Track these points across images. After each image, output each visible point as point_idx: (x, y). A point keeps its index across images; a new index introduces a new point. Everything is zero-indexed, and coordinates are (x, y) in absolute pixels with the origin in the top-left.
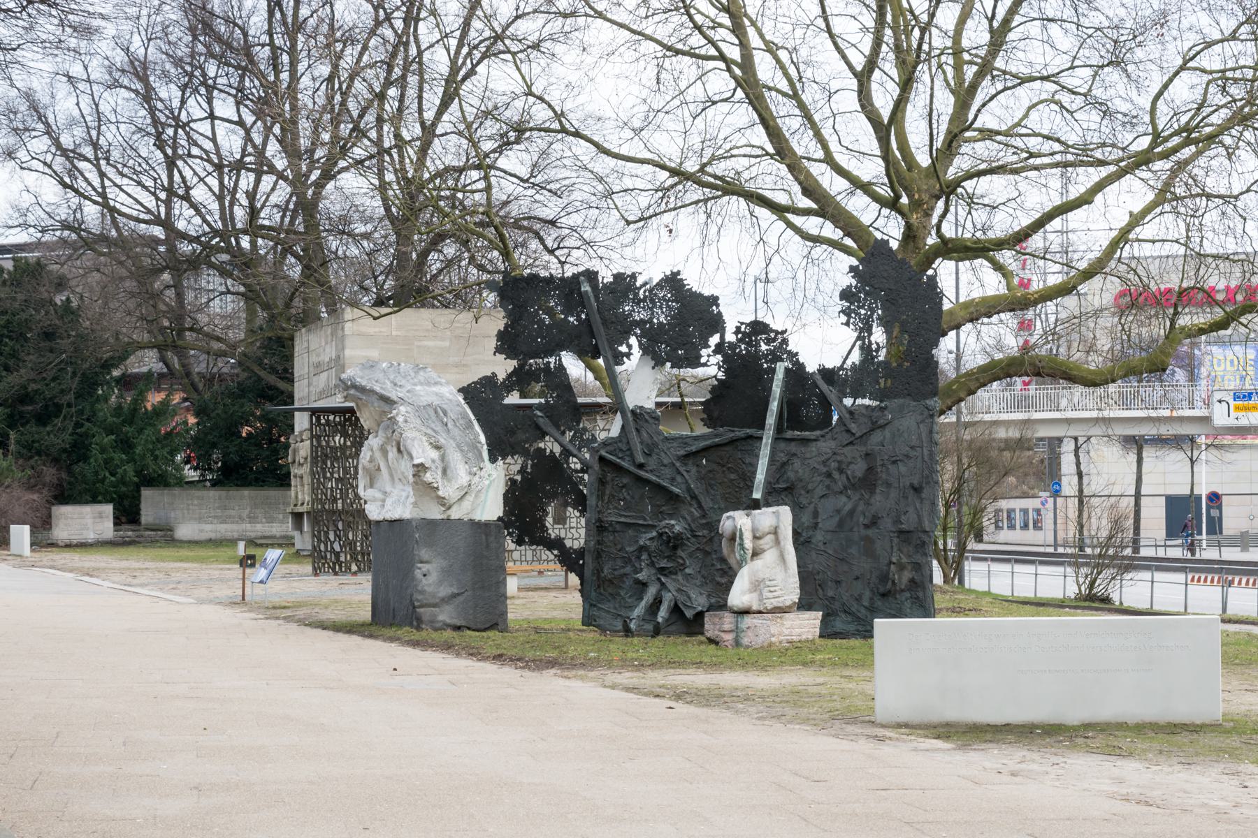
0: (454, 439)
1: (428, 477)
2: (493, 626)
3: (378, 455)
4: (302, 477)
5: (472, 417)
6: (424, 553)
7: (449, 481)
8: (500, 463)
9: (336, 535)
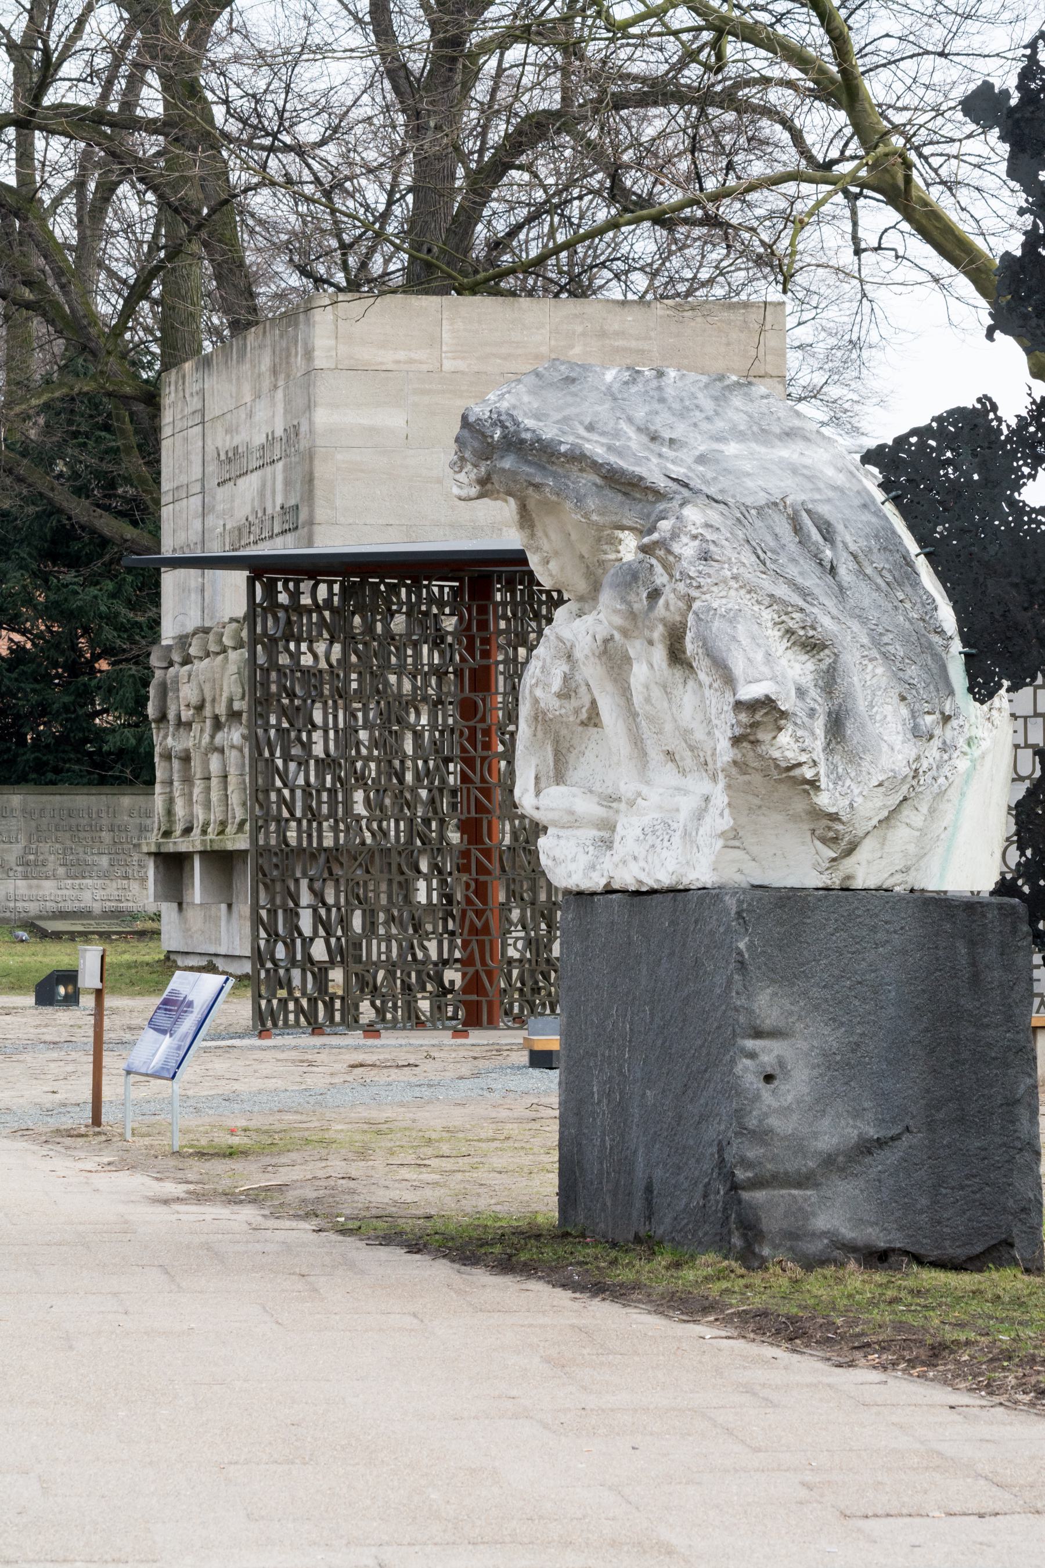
0: (863, 620)
1: (785, 745)
2: (994, 1254)
3: (592, 672)
4: (186, 759)
5: (912, 547)
6: (767, 1004)
7: (853, 758)
8: (1002, 699)
9: (317, 918)
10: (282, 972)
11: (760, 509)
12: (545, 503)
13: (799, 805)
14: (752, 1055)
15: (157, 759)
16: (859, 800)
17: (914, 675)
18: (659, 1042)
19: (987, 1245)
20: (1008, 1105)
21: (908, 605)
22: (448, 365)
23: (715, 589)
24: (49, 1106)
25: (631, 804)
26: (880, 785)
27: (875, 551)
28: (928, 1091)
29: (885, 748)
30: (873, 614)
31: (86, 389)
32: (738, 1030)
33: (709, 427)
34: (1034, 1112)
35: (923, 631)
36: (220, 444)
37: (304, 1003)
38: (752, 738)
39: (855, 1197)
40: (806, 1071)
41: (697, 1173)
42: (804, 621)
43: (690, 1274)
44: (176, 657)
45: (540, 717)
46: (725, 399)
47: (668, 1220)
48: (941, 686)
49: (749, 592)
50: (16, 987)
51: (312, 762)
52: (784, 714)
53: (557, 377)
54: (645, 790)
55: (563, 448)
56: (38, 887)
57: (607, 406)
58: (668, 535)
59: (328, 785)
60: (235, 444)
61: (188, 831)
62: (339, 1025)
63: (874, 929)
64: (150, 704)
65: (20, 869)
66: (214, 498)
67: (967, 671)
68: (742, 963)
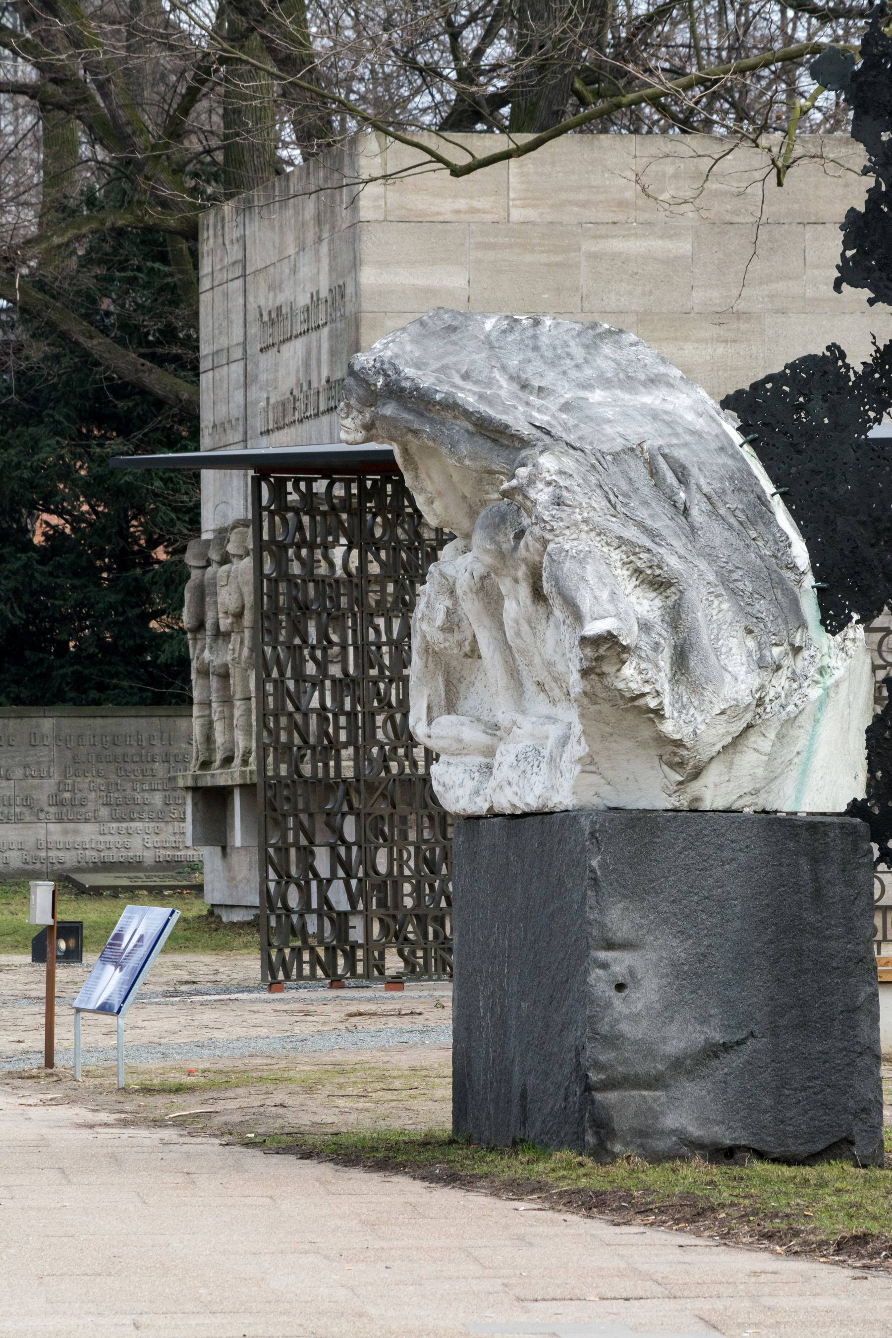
0: (712, 558)
1: (630, 677)
2: (837, 1149)
3: (470, 607)
4: (225, 676)
5: (769, 487)
6: (618, 918)
7: (696, 688)
8: (856, 632)
9: (335, 858)
10: (295, 918)
11: (616, 456)
12: (423, 448)
13: (646, 733)
14: (604, 966)
15: (193, 676)
16: (703, 727)
17: (762, 609)
18: (531, 957)
19: (828, 1143)
20: (849, 1011)
21: (760, 543)
22: (516, 215)
23: (567, 532)
24: (10, 1054)
25: (509, 732)
26: (723, 713)
27: (729, 492)
28: (772, 999)
29: (728, 678)
30: (723, 553)
31: (120, 223)
32: (591, 943)
33: (578, 374)
34: (876, 1018)
35: (775, 567)
36: (262, 303)
37: (321, 951)
38: (598, 670)
39: (703, 1098)
40: (656, 981)
41: (560, 1078)
42: (651, 561)
43: (541, 1166)
44: (214, 556)
45: (427, 649)
46: (596, 346)
47: (538, 1124)
48: (791, 618)
49: (599, 534)
50: (15, 947)
51: (328, 683)
52: (625, 649)
53: (440, 325)
54: (519, 718)
55: (438, 397)
56: (76, 832)
57: (483, 355)
58: (525, 481)
59: (348, 707)
60: (278, 304)
61: (228, 761)
62: (361, 976)
63: (720, 847)
64: (185, 610)
65: (53, 810)
66: (257, 366)
67: (820, 604)
68: (595, 880)
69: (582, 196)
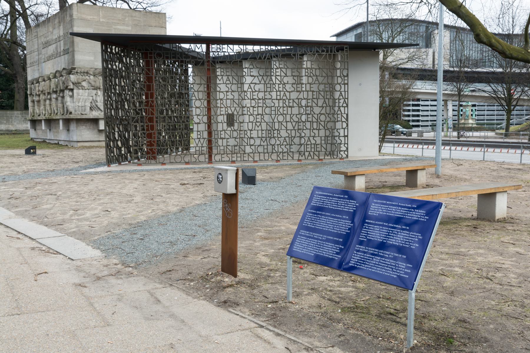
22: (101, 20)
69: (112, 18)
